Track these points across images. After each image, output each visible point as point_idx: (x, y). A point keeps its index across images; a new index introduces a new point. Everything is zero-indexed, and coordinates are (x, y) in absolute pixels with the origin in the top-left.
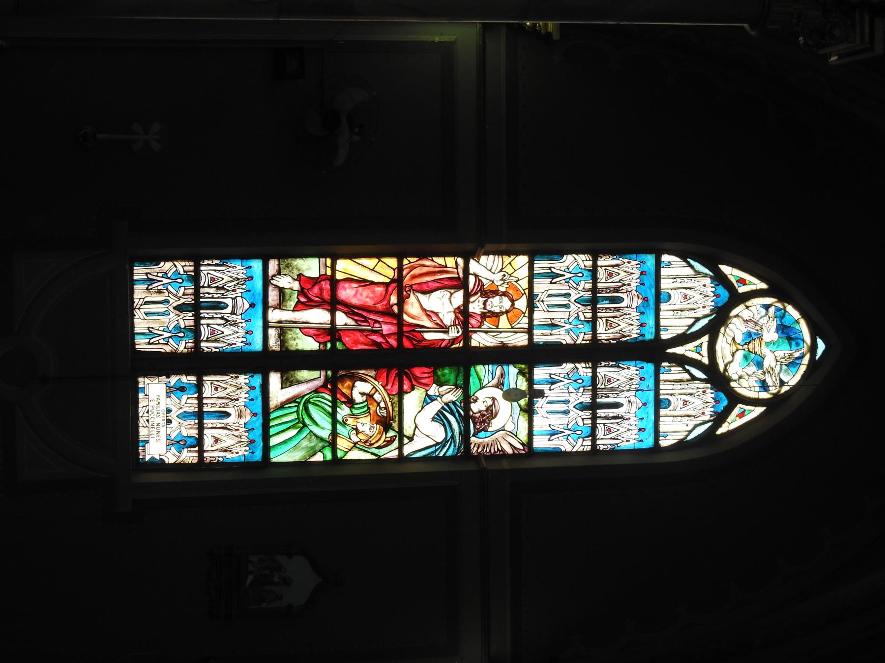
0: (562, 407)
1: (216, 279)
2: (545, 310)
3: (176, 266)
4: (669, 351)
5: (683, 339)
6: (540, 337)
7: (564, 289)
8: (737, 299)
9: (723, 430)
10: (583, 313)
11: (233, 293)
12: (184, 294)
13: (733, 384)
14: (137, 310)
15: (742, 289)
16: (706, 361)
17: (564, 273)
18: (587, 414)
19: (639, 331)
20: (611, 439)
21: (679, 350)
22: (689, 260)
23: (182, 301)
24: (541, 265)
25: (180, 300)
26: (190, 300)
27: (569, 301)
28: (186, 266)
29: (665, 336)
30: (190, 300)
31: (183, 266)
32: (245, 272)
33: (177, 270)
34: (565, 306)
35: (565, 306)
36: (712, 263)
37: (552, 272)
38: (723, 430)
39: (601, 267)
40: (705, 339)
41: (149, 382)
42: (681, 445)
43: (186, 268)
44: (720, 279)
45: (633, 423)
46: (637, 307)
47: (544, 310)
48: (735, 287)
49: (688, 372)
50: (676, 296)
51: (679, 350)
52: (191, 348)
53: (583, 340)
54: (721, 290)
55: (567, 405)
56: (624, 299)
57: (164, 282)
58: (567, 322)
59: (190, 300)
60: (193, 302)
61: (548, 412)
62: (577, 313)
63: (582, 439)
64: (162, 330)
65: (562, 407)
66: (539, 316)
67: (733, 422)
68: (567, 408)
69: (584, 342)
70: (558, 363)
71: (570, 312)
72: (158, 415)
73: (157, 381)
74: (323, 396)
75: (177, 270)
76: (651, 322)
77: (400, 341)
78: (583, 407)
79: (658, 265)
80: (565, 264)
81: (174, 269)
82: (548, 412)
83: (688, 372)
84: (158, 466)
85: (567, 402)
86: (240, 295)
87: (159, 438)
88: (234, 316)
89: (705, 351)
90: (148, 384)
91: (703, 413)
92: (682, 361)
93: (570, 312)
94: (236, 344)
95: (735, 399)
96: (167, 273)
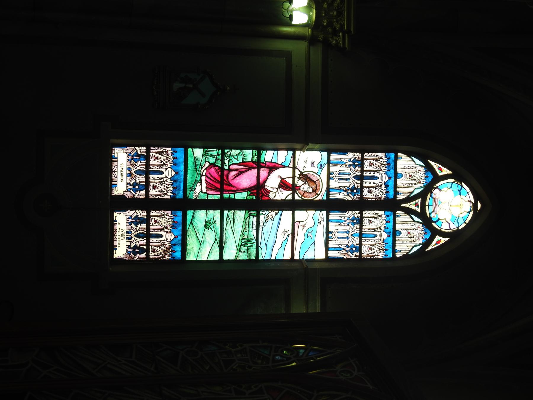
0: (345, 235)
2: (337, 181)
3: (136, 213)
5: (408, 199)
8: (437, 179)
9: (430, 248)
11: (167, 166)
12: (140, 165)
14: (113, 172)
15: (440, 174)
17: (348, 162)
19: (385, 226)
21: (406, 205)
22: (412, 157)
23: (139, 232)
24: (334, 157)
25: (138, 231)
26: (143, 168)
27: (350, 177)
28: (142, 149)
29: (399, 197)
30: (143, 168)
31: (140, 149)
33: (137, 151)
36: (424, 158)
37: (340, 247)
39: (365, 217)
40: (419, 201)
41: (117, 215)
42: (407, 256)
43: (142, 151)
44: (429, 168)
45: (382, 246)
47: (336, 181)
48: (437, 163)
50: (404, 233)
51: (406, 205)
53: (355, 256)
54: (428, 231)
56: (379, 178)
58: (349, 161)
59: (143, 168)
60: (145, 170)
61: (338, 238)
62: (354, 184)
64: (128, 218)
65: (345, 235)
68: (349, 178)
69: (356, 257)
70: (344, 211)
71: (349, 241)
73: (122, 214)
74: (214, 179)
75: (137, 151)
78: (356, 177)
80: (348, 215)
81: (136, 214)
82: (339, 179)
85: (349, 174)
86: (170, 167)
88: (167, 178)
90: (116, 216)
92: (409, 212)
93: (349, 241)
95: (435, 232)
96: (132, 216)
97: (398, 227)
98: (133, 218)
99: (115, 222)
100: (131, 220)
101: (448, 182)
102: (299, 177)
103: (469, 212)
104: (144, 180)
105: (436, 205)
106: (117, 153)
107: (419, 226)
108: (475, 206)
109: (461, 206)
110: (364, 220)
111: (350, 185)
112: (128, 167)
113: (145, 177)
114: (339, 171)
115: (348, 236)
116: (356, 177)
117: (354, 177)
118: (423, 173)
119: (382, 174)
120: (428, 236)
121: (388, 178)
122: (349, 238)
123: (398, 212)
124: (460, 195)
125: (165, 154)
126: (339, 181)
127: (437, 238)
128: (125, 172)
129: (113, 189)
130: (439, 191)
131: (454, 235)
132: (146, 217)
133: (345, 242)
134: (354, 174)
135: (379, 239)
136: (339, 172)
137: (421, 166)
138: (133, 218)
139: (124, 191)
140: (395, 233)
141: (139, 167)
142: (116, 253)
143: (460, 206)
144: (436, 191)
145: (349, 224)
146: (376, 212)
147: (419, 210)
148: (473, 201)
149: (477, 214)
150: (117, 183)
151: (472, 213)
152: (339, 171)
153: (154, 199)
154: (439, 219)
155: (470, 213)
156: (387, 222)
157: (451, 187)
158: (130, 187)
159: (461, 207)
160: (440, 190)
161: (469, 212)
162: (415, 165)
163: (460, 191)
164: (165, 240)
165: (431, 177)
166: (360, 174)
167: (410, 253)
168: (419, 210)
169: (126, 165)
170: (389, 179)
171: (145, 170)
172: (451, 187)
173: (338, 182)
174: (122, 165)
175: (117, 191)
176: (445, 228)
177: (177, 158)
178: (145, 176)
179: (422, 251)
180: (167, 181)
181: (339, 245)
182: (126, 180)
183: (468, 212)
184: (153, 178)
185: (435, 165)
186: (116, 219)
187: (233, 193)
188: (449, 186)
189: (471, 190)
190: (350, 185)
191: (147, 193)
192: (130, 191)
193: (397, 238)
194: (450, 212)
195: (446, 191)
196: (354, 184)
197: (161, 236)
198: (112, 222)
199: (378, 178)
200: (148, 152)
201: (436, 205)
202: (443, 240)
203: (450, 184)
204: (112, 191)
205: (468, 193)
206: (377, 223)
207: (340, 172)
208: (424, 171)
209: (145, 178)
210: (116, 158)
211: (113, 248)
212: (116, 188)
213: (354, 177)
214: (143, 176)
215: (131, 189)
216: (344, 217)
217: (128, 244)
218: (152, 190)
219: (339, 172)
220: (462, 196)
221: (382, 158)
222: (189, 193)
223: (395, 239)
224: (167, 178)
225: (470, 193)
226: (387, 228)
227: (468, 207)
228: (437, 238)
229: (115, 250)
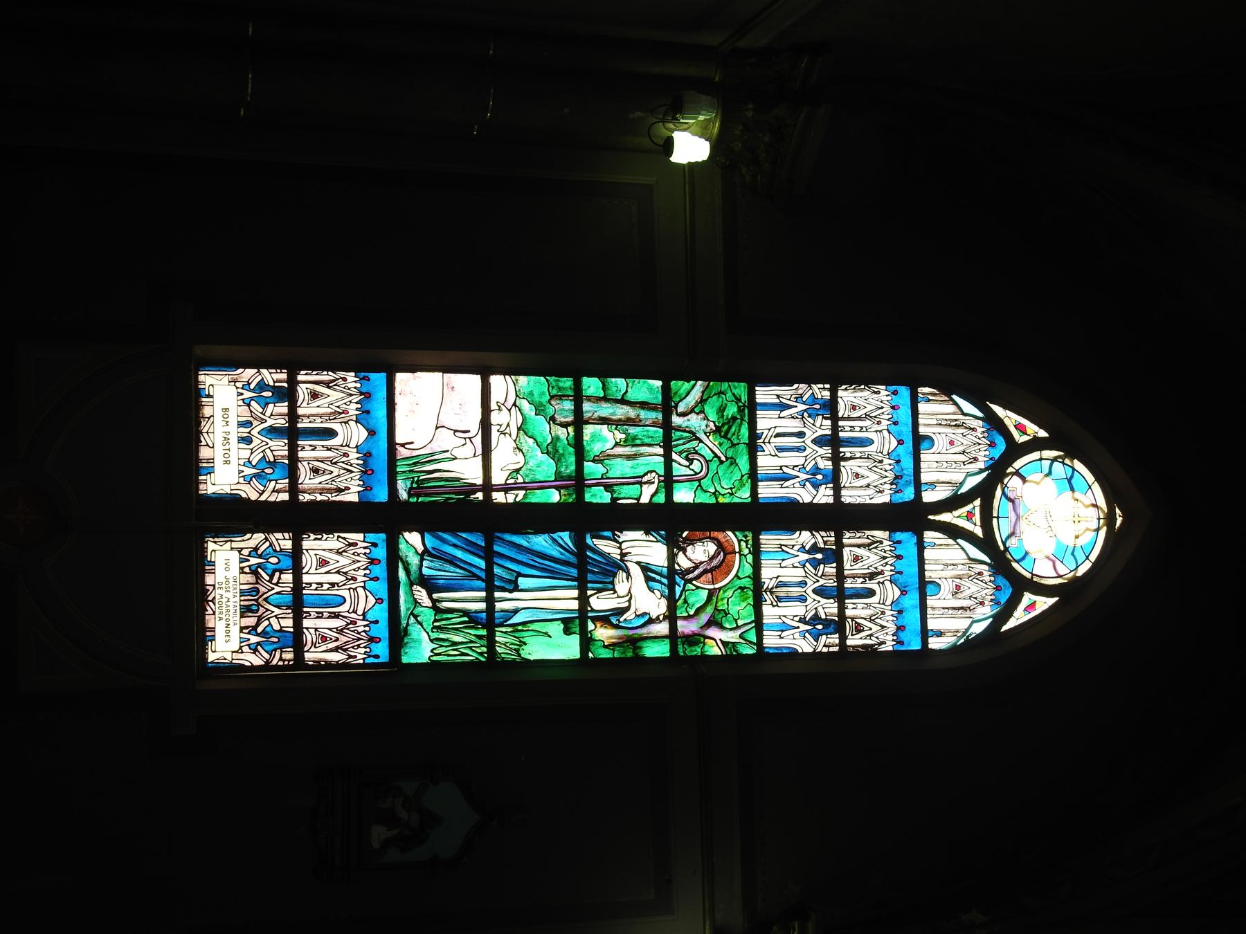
1: (328, 639)
4: (931, 517)
6: (768, 491)
7: (795, 425)
8: (1015, 451)
9: (1011, 624)
10: (823, 608)
11: (352, 582)
13: (1015, 565)
16: (979, 532)
17: (799, 553)
18: (827, 451)
20: (861, 638)
21: (945, 517)
26: (282, 422)
29: (928, 497)
30: (282, 422)
32: (358, 385)
34: (798, 449)
35: (798, 449)
38: (1011, 624)
40: (979, 532)
44: (995, 424)
46: (893, 603)
49: (955, 404)
51: (945, 517)
52: (289, 661)
54: (1002, 581)
55: (804, 590)
57: (251, 642)
63: (821, 416)
66: (765, 462)
67: (1019, 617)
68: (803, 444)
71: (806, 457)
72: (225, 442)
73: (228, 545)
76: (912, 618)
77: (578, 387)
78: (819, 441)
79: (921, 547)
83: (955, 404)
84: (232, 670)
85: (801, 435)
87: (225, 448)
89: (977, 518)
90: (213, 551)
91: (975, 459)
92: (954, 532)
94: (356, 657)
95: (1022, 585)
97: (931, 572)
98: (252, 386)
99: (208, 634)
100: (248, 394)
101: (1041, 459)
102: (681, 553)
103: (1098, 530)
104: (286, 453)
105: (1018, 517)
106: (215, 551)
107: (979, 571)
108: (1110, 519)
109: (1077, 519)
110: (846, 551)
111: (807, 611)
112: (241, 419)
113: (286, 444)
114: (777, 578)
115: (804, 594)
116: (819, 441)
117: (815, 441)
118: (987, 579)
119: (883, 583)
120: (1004, 597)
121: (900, 593)
122: (805, 449)
123: (929, 536)
124: (1072, 489)
125: (338, 386)
126: (779, 454)
127: (1028, 598)
128: (234, 432)
129: (204, 477)
130: (1022, 483)
131: (1068, 591)
132: (285, 385)
133: (795, 459)
134: (815, 582)
135: (881, 602)
136: (778, 580)
137: (977, 418)
138: (252, 386)
139: (233, 652)
140: (919, 441)
141: (269, 417)
142: (214, 650)
143: (1074, 519)
144: (1014, 482)
145: (805, 485)
146: (868, 533)
147: (978, 502)
148: (1102, 502)
149: (1114, 541)
150: (214, 569)
151: (1103, 533)
152: (777, 578)
153: (313, 503)
154: (1027, 553)
155: (1100, 532)
156: (893, 408)
157: (1050, 473)
158: (248, 394)
159: (1076, 522)
160: (1024, 479)
161: (1098, 530)
162: (961, 417)
163: (1069, 480)
164: (344, 444)
165: (1001, 446)
166: (830, 451)
167: (958, 644)
168: (978, 502)
169: (237, 412)
170: (902, 593)
171: (287, 425)
172: (1050, 473)
173: (776, 455)
174: (228, 589)
175: (215, 651)
176: (1044, 571)
177: (373, 471)
178: (286, 441)
179: (558, 502)
180: (346, 455)
181: (781, 467)
182: (236, 622)
183: (1095, 530)
184: (309, 451)
185: (1010, 418)
186: (211, 394)
187: (509, 486)
188: (1046, 471)
189: (1098, 479)
190: (807, 611)
191: (294, 489)
192: (249, 405)
193: (931, 602)
194: (1051, 534)
195: (1037, 483)
196: (816, 609)
197: (331, 433)
198: (201, 565)
199: (871, 442)
200: (293, 382)
201: (1018, 517)
202: (1044, 603)
203: (1046, 464)
204: (198, 483)
205: (1090, 487)
206: (871, 559)
207: (780, 579)
208: (990, 576)
209: (286, 448)
210: (213, 564)
211: (202, 636)
212: (213, 642)
213: (815, 441)
214: (286, 535)
215: (252, 399)
216: (792, 618)
217: (246, 454)
218: (310, 479)
219: (778, 580)
220: (1077, 495)
221: (881, 543)
222: (406, 622)
223: (920, 458)
224: (348, 446)
225: (1097, 488)
226: (900, 573)
227: (1092, 518)
228: (1028, 598)
229: (211, 641)
